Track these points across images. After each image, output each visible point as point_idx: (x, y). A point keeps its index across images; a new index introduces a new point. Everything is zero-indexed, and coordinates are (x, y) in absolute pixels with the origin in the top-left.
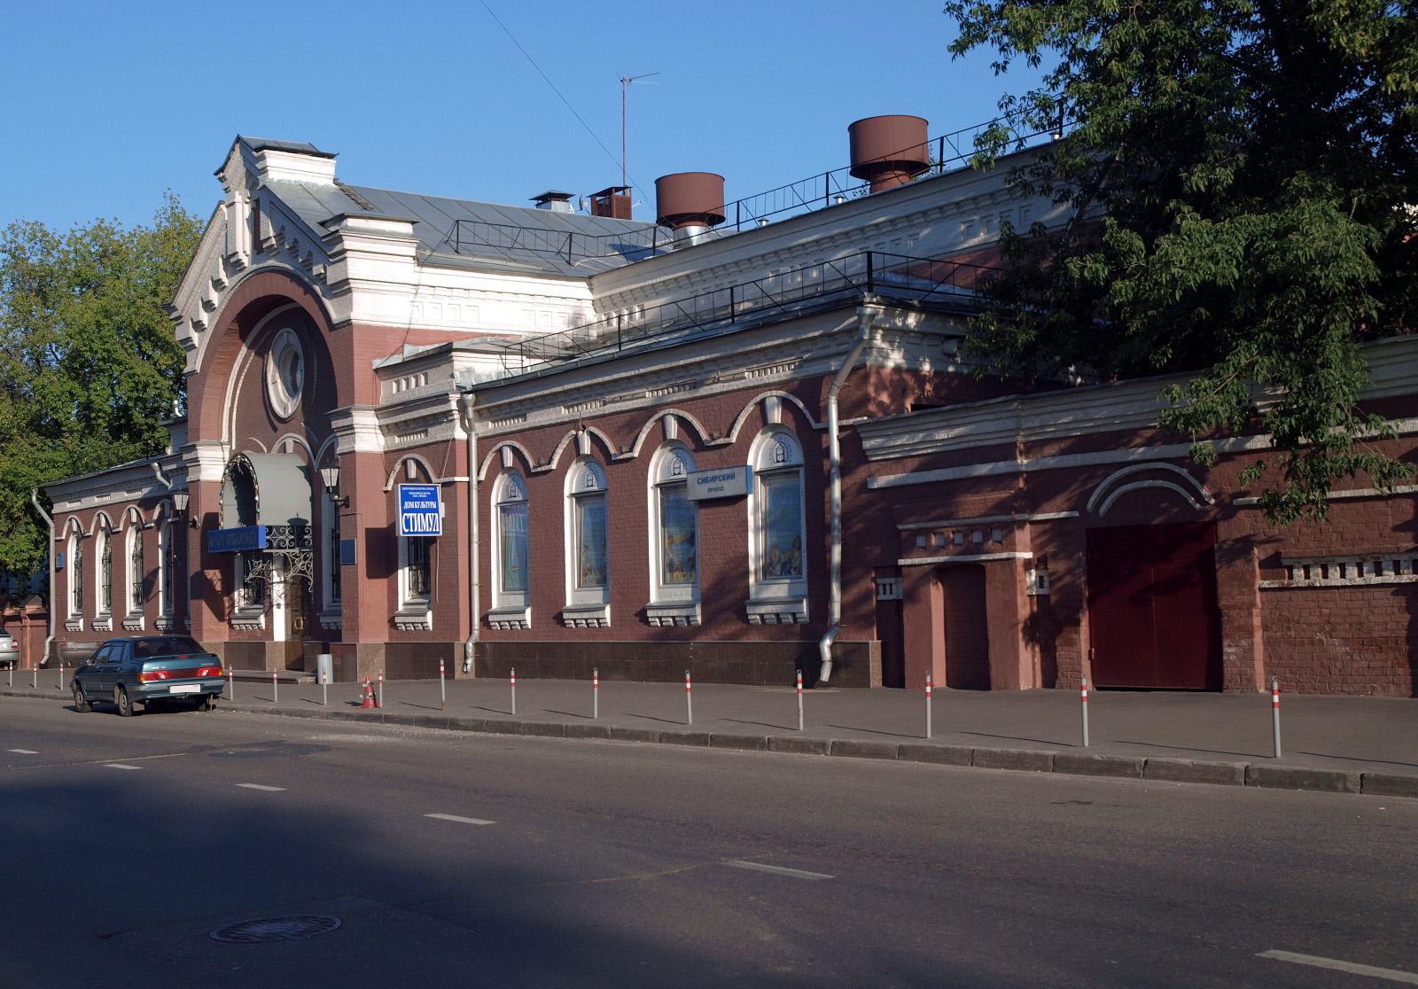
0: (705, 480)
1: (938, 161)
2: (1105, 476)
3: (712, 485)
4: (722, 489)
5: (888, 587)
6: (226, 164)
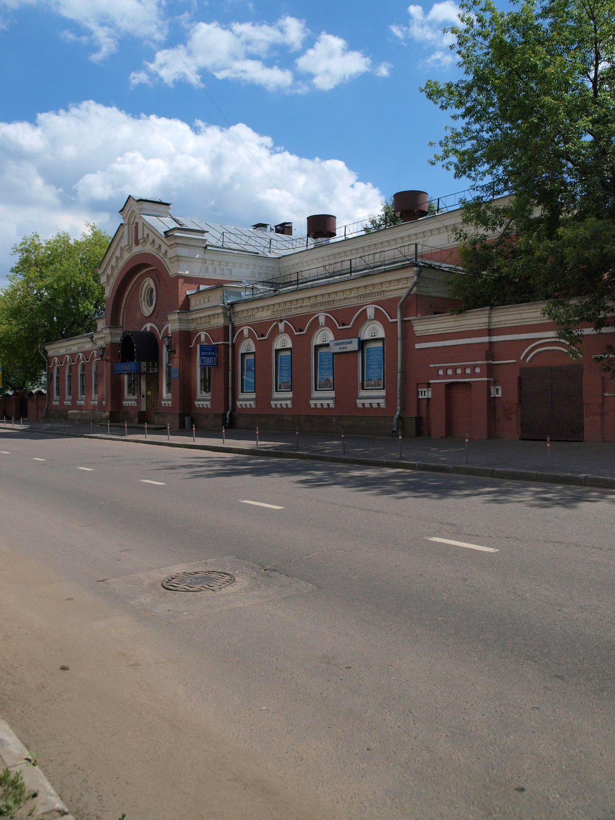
0: (338, 344)
1: (436, 209)
2: (146, 268)
3: (341, 346)
4: (346, 348)
5: (423, 392)
6: (124, 208)
